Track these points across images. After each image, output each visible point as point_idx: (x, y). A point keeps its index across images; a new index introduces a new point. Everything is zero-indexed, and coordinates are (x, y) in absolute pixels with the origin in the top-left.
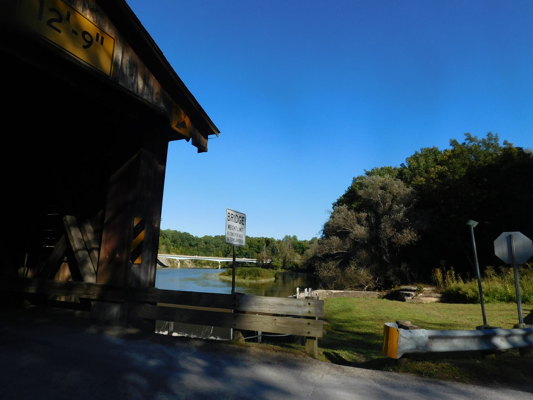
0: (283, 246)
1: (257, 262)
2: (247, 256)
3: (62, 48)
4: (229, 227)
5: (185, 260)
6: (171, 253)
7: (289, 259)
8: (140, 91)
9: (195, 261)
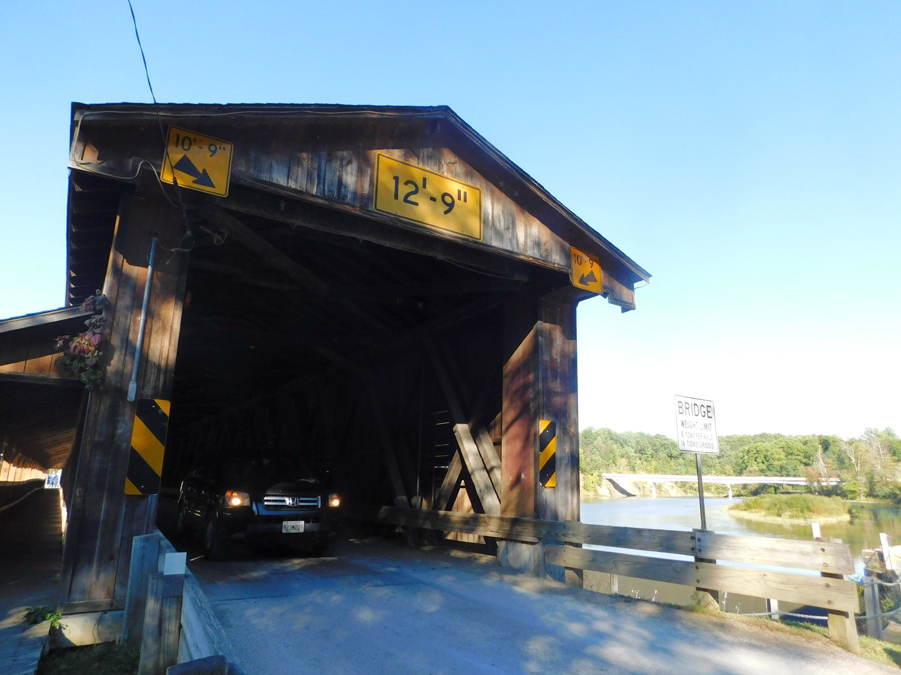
0: (861, 449)
2: (784, 472)
4: (683, 424)
6: (638, 471)
7: (882, 477)
8: (521, 246)
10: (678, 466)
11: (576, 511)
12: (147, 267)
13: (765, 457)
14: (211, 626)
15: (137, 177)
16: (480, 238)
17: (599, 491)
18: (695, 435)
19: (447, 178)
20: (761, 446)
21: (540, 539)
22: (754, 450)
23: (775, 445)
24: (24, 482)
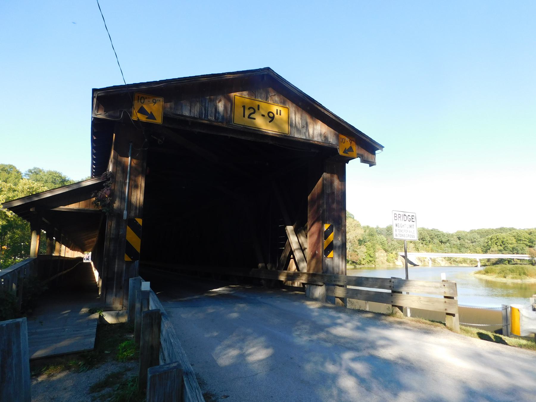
1: (530, 258)
3: (258, 128)
4: (396, 225)
5: (437, 258)
8: (311, 136)
9: (449, 259)
10: (446, 248)
11: (344, 270)
12: (128, 158)
13: (502, 242)
14: (158, 304)
15: (120, 119)
16: (288, 133)
17: (396, 263)
18: (404, 231)
19: (270, 104)
20: (500, 235)
21: (324, 283)
22: (495, 238)
23: (509, 234)
24: (75, 258)
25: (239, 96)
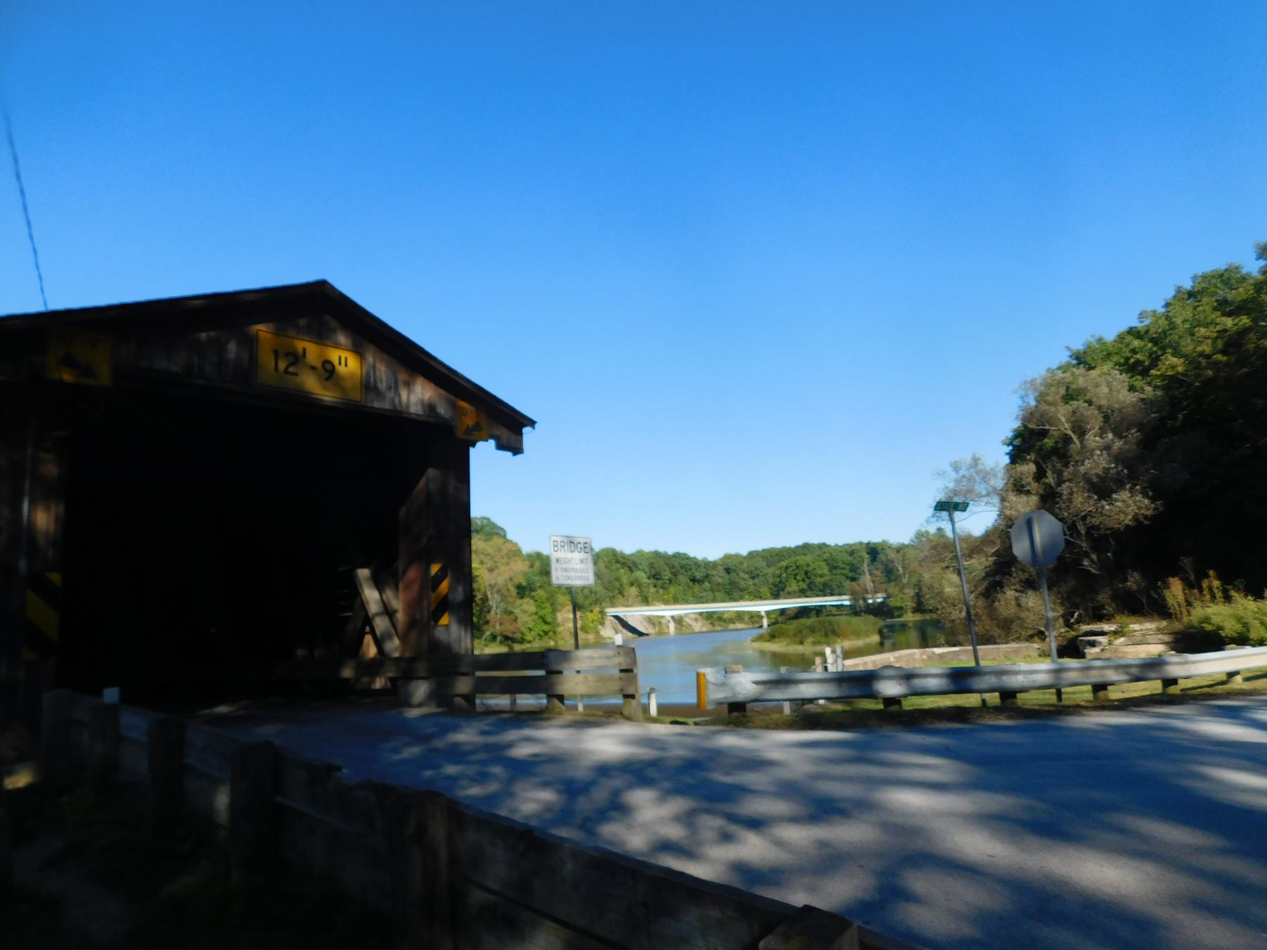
4: (557, 561)
9: (709, 617)
13: (806, 573)
20: (802, 560)
22: (793, 565)
25: (266, 332)
